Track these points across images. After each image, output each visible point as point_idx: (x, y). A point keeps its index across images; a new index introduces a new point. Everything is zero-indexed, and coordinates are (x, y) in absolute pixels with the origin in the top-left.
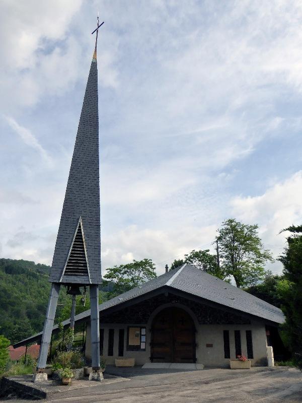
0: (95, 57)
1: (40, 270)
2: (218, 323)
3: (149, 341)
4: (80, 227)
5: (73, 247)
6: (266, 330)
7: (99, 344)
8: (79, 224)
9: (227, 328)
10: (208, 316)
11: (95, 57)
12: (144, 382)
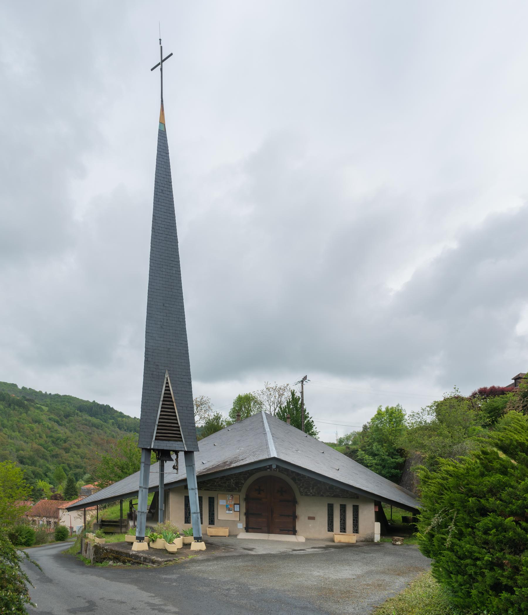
0: (162, 123)
1: (28, 397)
2: (322, 496)
3: (244, 510)
4: (167, 383)
5: (162, 408)
6: (375, 505)
7: (199, 515)
8: (165, 380)
9: (331, 501)
10: (311, 488)
11: (162, 123)
12: (375, 548)
